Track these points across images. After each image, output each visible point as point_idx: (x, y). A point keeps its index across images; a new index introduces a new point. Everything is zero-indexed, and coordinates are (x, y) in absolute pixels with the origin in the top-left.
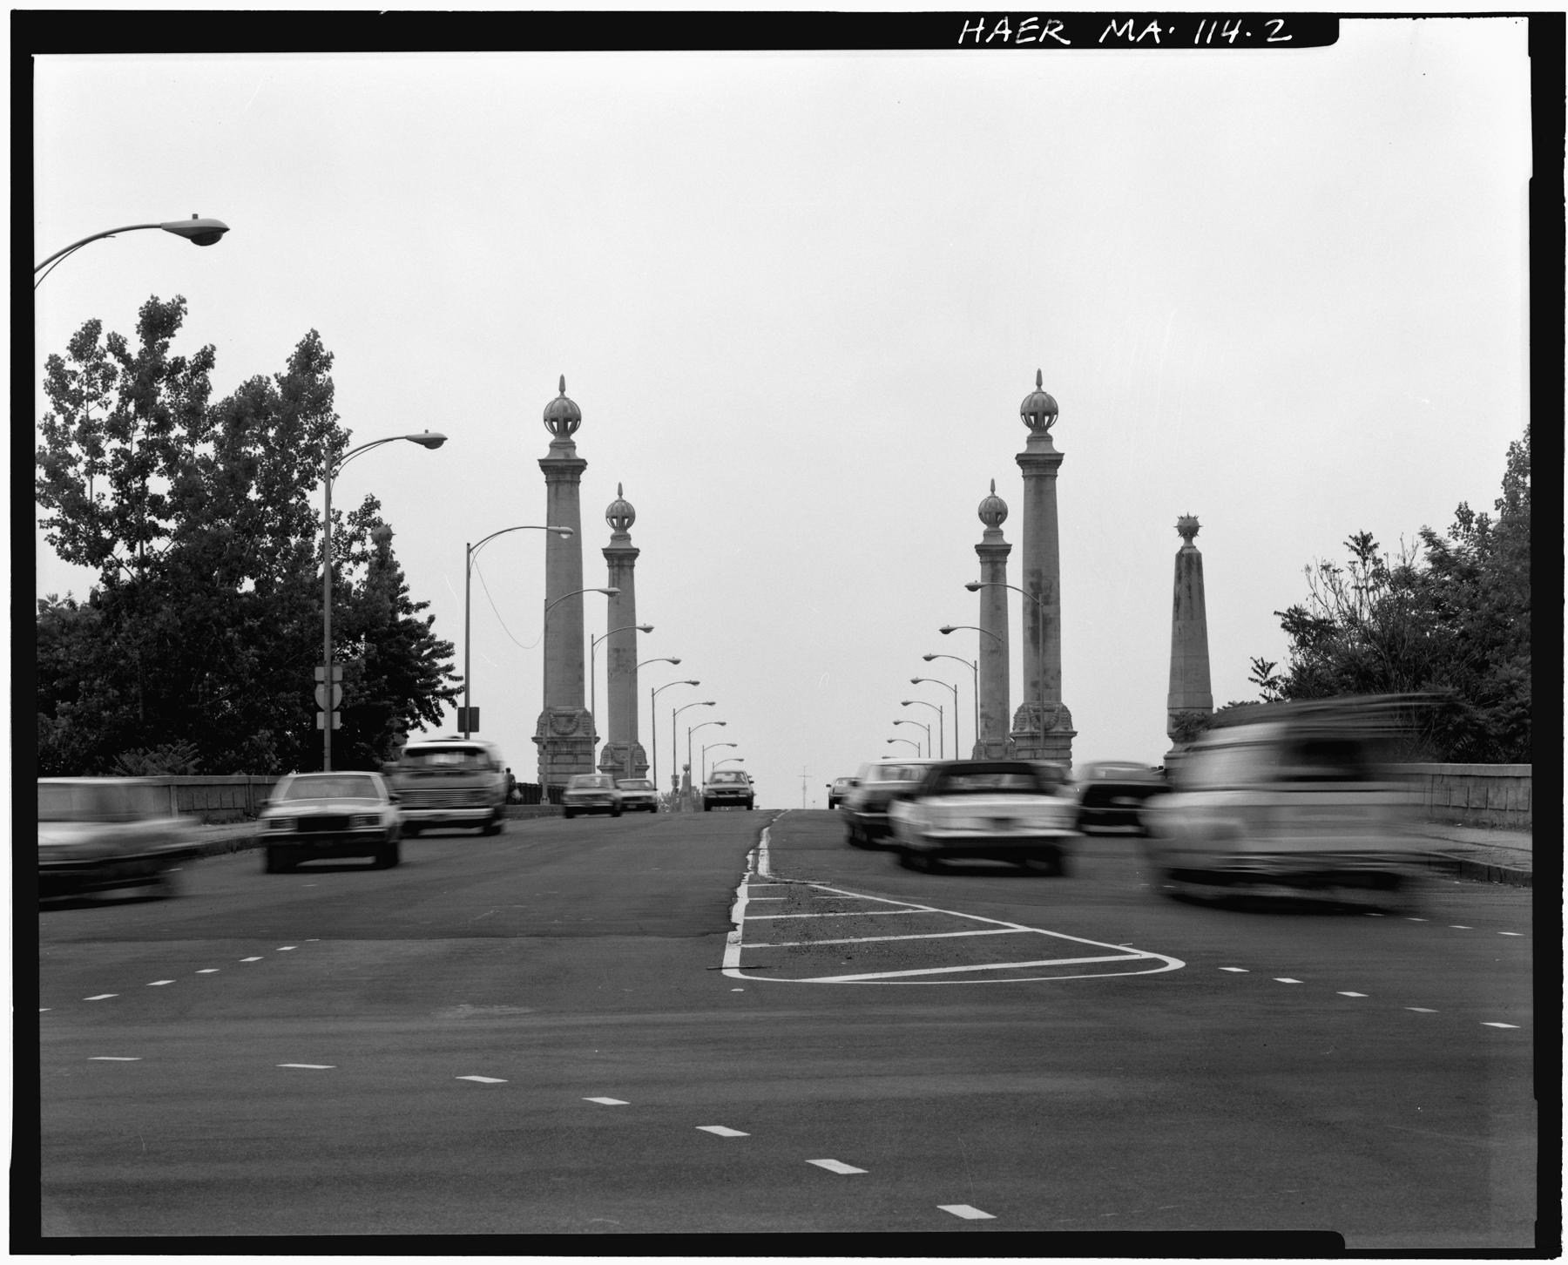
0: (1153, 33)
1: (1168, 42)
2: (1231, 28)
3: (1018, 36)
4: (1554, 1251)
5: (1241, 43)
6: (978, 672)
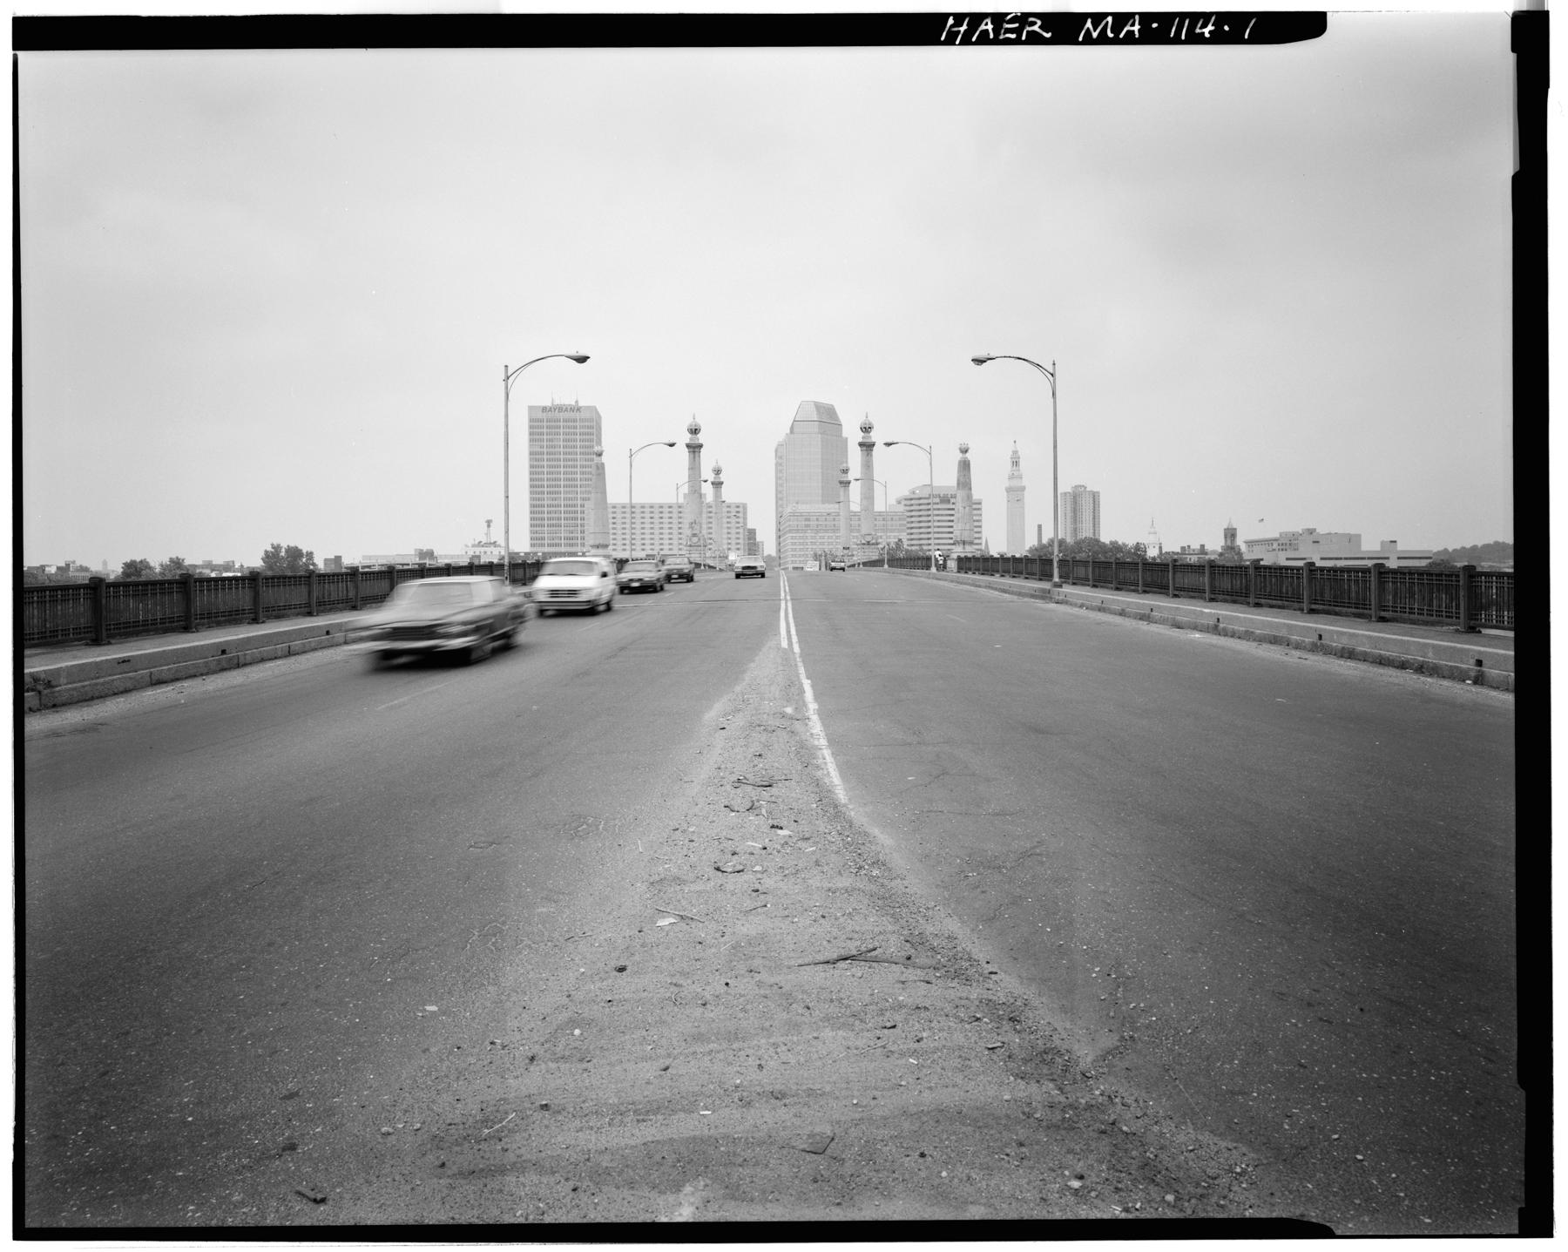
0: (987, 30)
1: (1218, 38)
2: (1204, 26)
6: (1408, 679)
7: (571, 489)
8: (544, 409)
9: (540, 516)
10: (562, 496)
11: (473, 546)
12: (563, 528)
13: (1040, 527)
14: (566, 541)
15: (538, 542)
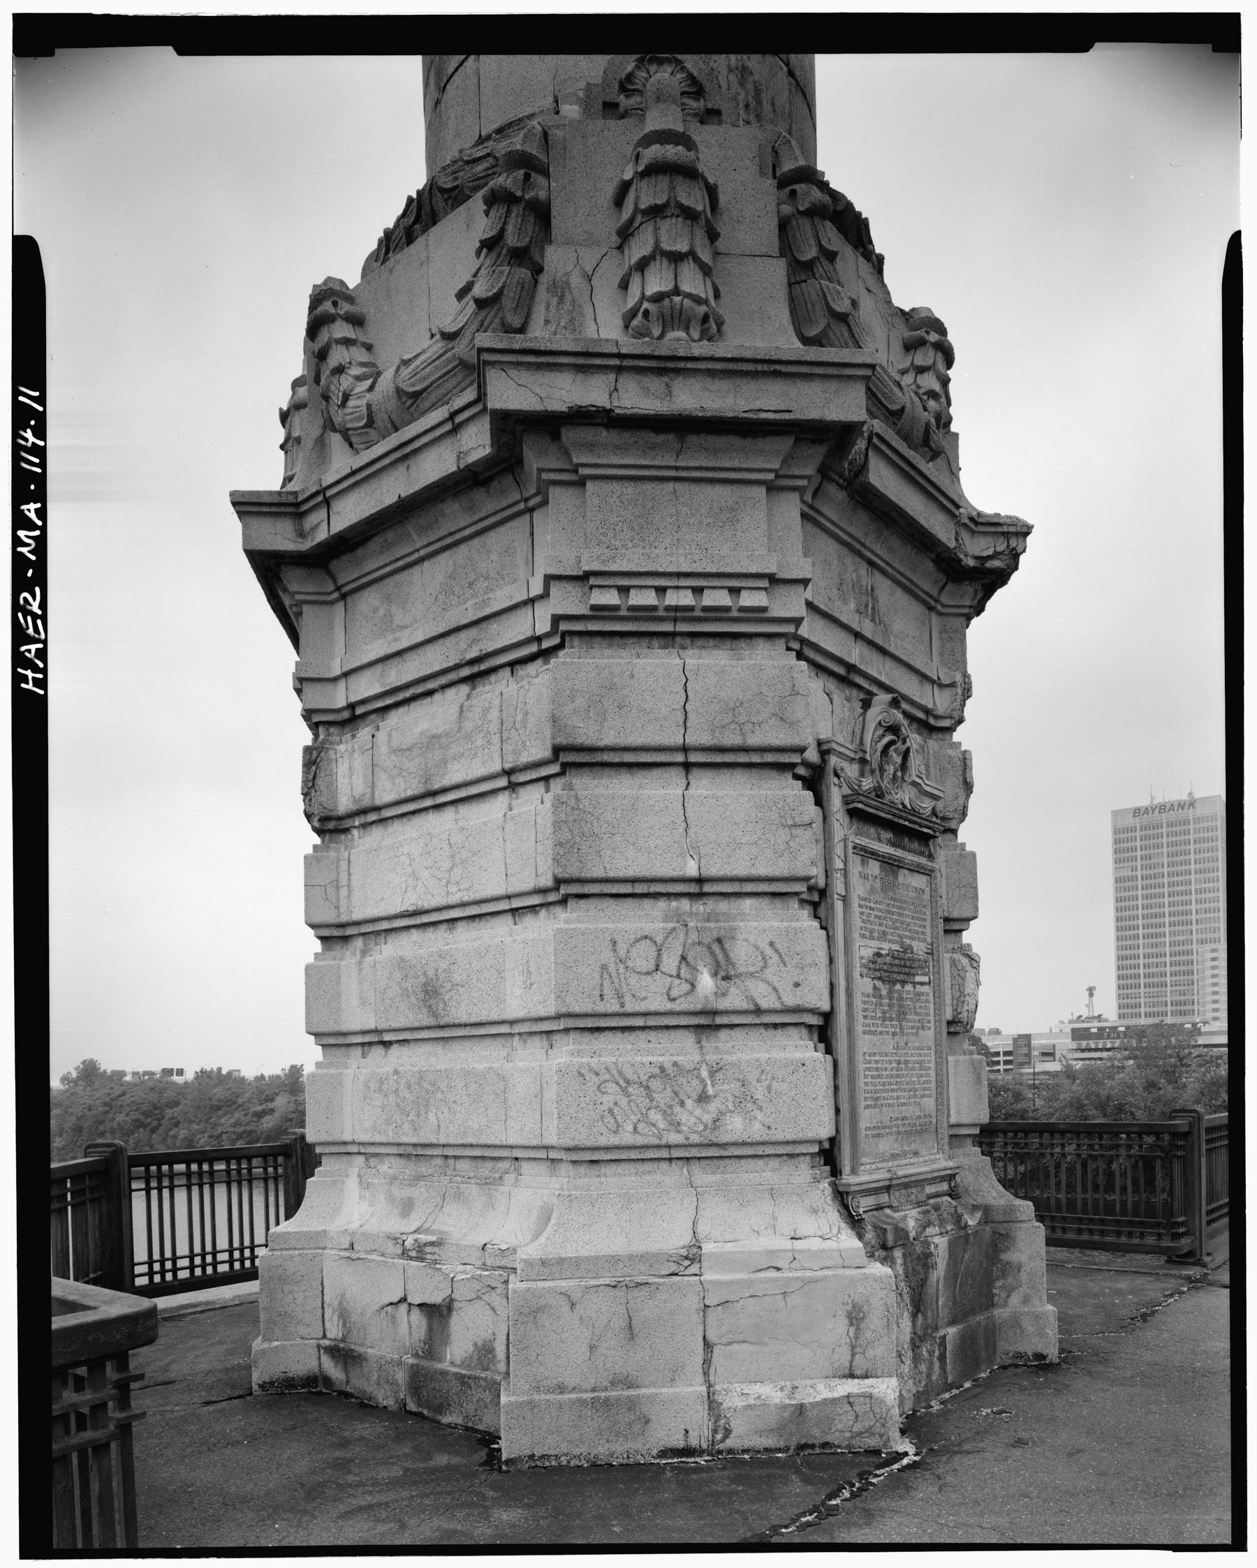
0: (37, 649)
2: (26, 440)
3: (36, 636)
4: (1238, 1542)
5: (41, 432)
7: (1181, 928)
8: (1137, 812)
9: (1133, 971)
10: (1167, 939)
11: (1071, 1022)
12: (1169, 988)
13: (1235, 244)
14: (1174, 1008)
15: (1130, 1011)
